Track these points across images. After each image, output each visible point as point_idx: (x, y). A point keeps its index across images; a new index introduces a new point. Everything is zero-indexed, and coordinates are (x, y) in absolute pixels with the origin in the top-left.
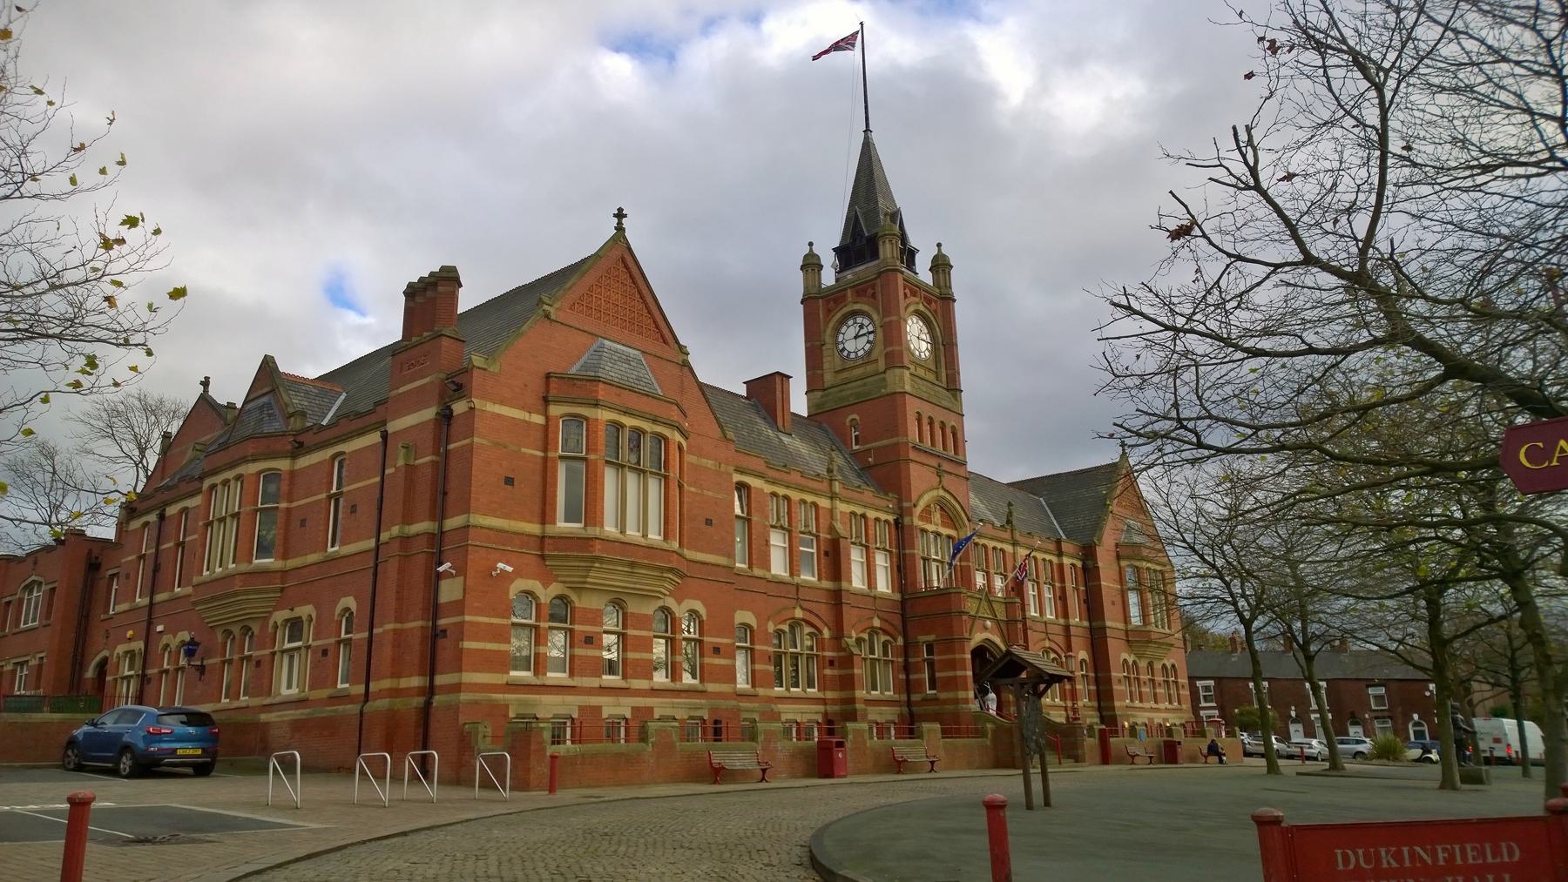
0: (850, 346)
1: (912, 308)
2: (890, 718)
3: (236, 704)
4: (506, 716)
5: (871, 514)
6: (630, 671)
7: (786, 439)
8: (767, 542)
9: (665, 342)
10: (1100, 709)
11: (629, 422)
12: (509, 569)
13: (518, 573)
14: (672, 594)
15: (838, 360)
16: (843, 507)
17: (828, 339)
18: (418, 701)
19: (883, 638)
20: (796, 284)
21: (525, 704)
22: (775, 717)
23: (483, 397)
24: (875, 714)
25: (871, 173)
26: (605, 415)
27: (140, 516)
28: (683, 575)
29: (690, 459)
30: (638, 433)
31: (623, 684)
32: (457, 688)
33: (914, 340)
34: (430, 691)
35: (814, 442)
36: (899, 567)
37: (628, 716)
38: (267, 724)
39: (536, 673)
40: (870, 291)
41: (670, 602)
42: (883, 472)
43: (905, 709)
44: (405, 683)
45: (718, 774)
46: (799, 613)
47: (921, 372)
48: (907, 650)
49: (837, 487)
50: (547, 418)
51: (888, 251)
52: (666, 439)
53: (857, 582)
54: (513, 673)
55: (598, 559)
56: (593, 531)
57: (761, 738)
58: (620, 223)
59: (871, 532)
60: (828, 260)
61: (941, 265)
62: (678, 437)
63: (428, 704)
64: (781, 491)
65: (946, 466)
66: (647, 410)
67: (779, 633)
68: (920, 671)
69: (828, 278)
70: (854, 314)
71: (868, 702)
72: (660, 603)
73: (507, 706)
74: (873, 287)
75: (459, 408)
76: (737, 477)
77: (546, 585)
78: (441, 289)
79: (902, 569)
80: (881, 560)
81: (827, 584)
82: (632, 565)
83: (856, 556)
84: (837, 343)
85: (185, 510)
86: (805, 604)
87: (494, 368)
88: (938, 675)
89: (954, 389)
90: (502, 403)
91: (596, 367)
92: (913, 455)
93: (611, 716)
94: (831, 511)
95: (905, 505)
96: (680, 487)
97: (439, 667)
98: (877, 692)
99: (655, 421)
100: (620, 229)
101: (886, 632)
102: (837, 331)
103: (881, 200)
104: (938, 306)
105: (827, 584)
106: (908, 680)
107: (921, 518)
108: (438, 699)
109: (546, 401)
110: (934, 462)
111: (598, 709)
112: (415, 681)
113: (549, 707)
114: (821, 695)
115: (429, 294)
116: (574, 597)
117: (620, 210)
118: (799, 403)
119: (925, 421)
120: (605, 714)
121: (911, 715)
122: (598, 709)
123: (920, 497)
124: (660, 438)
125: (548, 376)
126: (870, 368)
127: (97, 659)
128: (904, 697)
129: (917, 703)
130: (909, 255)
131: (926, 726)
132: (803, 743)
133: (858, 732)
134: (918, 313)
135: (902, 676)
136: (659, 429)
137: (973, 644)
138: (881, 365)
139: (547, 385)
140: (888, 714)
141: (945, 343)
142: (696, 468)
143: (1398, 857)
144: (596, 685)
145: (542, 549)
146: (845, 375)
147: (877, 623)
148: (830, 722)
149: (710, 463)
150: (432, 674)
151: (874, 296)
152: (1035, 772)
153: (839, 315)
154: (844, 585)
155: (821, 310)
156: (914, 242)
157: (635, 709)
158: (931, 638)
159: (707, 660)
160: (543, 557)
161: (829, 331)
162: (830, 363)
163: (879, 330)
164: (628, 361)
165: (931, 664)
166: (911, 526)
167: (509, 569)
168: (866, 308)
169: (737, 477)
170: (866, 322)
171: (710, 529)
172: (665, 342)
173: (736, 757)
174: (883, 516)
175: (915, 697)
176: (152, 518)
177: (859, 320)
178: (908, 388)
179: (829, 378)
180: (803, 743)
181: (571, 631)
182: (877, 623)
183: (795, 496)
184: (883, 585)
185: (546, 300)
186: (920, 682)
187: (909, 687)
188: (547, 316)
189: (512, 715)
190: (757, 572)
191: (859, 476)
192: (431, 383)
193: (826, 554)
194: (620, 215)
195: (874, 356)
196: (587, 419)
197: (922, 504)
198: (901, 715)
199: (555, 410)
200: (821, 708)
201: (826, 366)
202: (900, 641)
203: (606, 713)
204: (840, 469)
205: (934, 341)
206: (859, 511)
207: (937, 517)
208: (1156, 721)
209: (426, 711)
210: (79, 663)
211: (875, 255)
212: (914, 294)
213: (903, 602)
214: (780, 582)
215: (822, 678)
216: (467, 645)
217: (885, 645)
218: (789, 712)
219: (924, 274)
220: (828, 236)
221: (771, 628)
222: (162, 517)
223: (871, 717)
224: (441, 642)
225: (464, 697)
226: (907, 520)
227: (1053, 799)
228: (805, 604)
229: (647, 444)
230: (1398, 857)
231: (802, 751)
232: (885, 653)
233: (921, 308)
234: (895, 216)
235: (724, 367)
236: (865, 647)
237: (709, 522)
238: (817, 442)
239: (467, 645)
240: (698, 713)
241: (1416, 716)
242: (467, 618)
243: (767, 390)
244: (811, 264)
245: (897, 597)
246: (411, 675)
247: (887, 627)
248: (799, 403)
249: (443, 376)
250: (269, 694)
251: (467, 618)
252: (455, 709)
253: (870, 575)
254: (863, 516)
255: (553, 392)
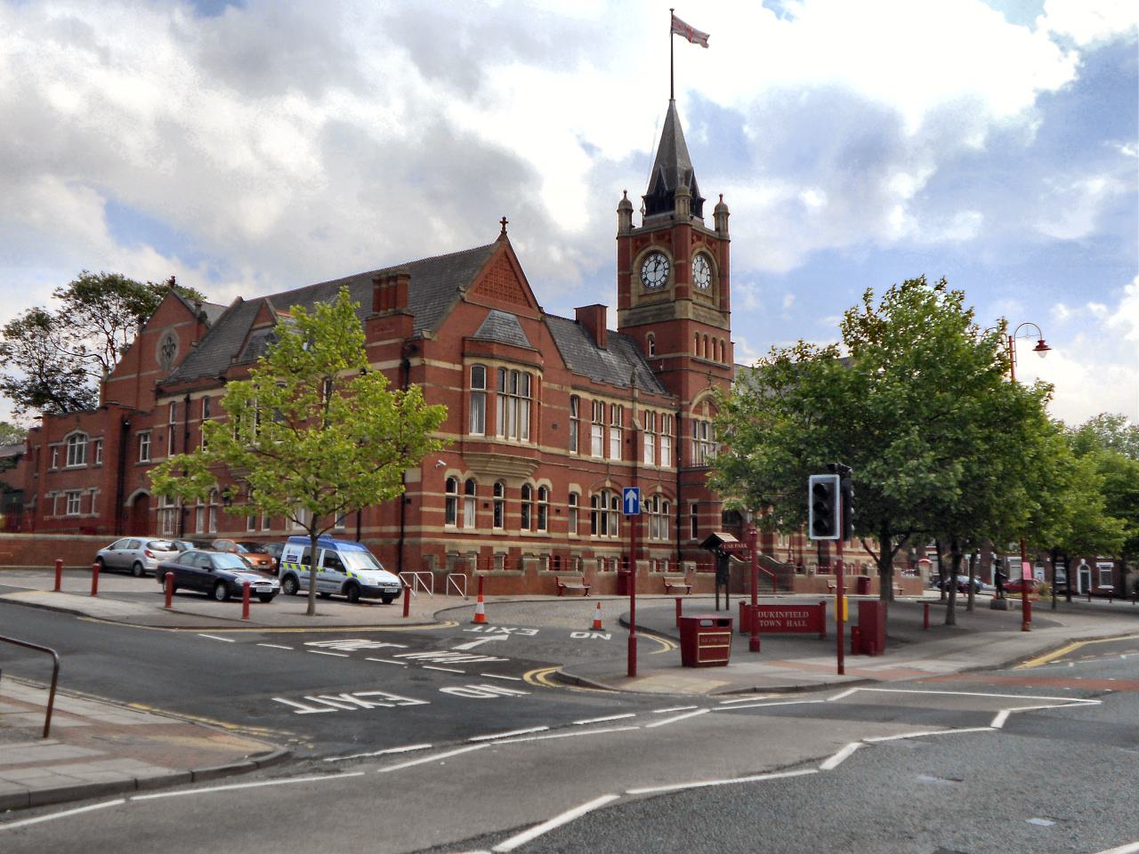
0: (651, 277)
1: (697, 251)
2: (665, 556)
3: (259, 534)
4: (443, 551)
5: (660, 411)
6: (508, 525)
7: (602, 354)
8: (590, 435)
9: (530, 306)
10: (819, 553)
11: (511, 367)
12: (444, 464)
13: (450, 465)
14: (532, 475)
15: (641, 287)
16: (640, 407)
17: (635, 270)
18: (395, 541)
19: (664, 500)
20: (613, 224)
21: (453, 544)
22: (590, 555)
23: (430, 358)
24: (655, 553)
25: (673, 118)
26: (497, 364)
27: (169, 395)
28: (538, 467)
29: (544, 384)
30: (515, 373)
31: (503, 533)
32: (419, 534)
33: (697, 274)
34: (402, 535)
35: (621, 353)
36: (677, 448)
37: (507, 553)
38: (849, 617)
39: (458, 526)
40: (667, 237)
41: (531, 481)
42: (669, 378)
43: (676, 551)
44: (385, 529)
45: (561, 591)
46: (608, 484)
47: (701, 300)
48: (680, 508)
49: (637, 393)
50: (464, 366)
51: (682, 208)
52: (531, 375)
53: (648, 461)
54: (446, 525)
55: (493, 456)
56: (490, 439)
57: (585, 569)
58: (504, 228)
59: (659, 424)
60: (638, 205)
61: (721, 213)
62: (538, 373)
63: (401, 543)
64: (600, 399)
65: (715, 372)
66: (521, 358)
67: (594, 499)
68: (688, 524)
69: (637, 220)
70: (655, 253)
71: (651, 545)
72: (525, 481)
73: (444, 546)
74: (670, 234)
75: (415, 362)
76: (573, 392)
77: (463, 472)
78: (399, 282)
79: (679, 450)
80: (665, 443)
81: (628, 463)
82: (512, 459)
83: (648, 441)
84: (641, 274)
85: (207, 399)
86: (613, 478)
87: (435, 339)
88: (699, 527)
89: (724, 311)
90: (439, 359)
91: (491, 331)
92: (691, 366)
93: (498, 553)
94: (632, 411)
95: (684, 403)
96: (539, 404)
97: (407, 521)
98: (659, 532)
99: (526, 365)
100: (504, 232)
101: (665, 496)
102: (642, 264)
103: (679, 160)
104: (718, 244)
105: (628, 463)
106: (679, 530)
107: (695, 411)
108: (406, 540)
109: (463, 355)
110: (706, 370)
111: (490, 548)
112: (393, 529)
113: (465, 545)
114: (620, 540)
115: (391, 283)
116: (478, 479)
117: (504, 219)
118: (612, 322)
119: (702, 338)
120: (494, 552)
121: (680, 554)
122: (490, 548)
123: (694, 397)
124: (527, 375)
125: (464, 339)
126: (664, 296)
127: (136, 493)
128: (675, 542)
129: (684, 547)
130: (697, 204)
131: (686, 563)
132: (610, 573)
133: (644, 568)
134: (702, 254)
135: (675, 527)
136: (528, 370)
137: (724, 507)
138: (672, 296)
139: (463, 345)
140: (666, 553)
141: (720, 277)
142: (548, 391)
143: (775, 614)
144: (490, 533)
145: (461, 450)
146: (646, 299)
147: (659, 489)
148: (625, 559)
149: (555, 386)
150: (403, 524)
151: (670, 241)
152: (722, 596)
153: (643, 253)
154: (639, 464)
155: (632, 245)
156: (703, 192)
157: (511, 549)
158: (696, 501)
159: (552, 518)
160: (462, 455)
161: (636, 264)
162: (635, 289)
163: (672, 269)
164: (508, 324)
165: (695, 520)
166: (687, 419)
167: (444, 464)
168: (663, 250)
169: (573, 392)
170: (663, 260)
171: (556, 432)
172: (530, 306)
173: (572, 580)
174: (668, 412)
175: (683, 542)
176: (180, 399)
177: (652, 258)
178: (690, 316)
179: (634, 301)
180: (610, 573)
181: (476, 500)
182: (659, 489)
183: (609, 401)
184: (666, 463)
185: (462, 289)
186: (687, 532)
187: (679, 535)
188: (463, 300)
189: (446, 551)
190: (584, 457)
191: (653, 379)
192: (396, 344)
193: (628, 441)
194: (504, 222)
195: (667, 287)
196: (487, 367)
197: (696, 402)
198: (673, 555)
199: (469, 362)
200: (620, 549)
201: (633, 291)
202: (675, 502)
203: (495, 551)
204: (640, 376)
205: (712, 274)
206: (651, 409)
207: (706, 410)
208: (862, 562)
209: (400, 546)
210: (121, 496)
211: (672, 207)
212: (699, 239)
213: (679, 474)
214: (596, 464)
215: (622, 528)
216: (425, 509)
217: (664, 505)
218: (600, 551)
219: (709, 222)
220: (638, 190)
221: (590, 494)
222: (188, 400)
223: (652, 556)
224: (408, 506)
225: (423, 540)
226: (684, 414)
227: (730, 608)
228: (613, 478)
229: (520, 380)
230: (775, 614)
231: (608, 578)
232: (665, 511)
233: (704, 249)
234: (689, 177)
235: (559, 302)
236: (651, 506)
237: (554, 426)
238: (623, 353)
239: (425, 509)
240: (546, 552)
241: (1083, 561)
242: (424, 493)
243: (590, 318)
244: (625, 209)
245: (675, 470)
246: (389, 525)
247: (666, 492)
248: (612, 322)
249: (403, 340)
250: (284, 529)
251: (424, 493)
252: (419, 547)
253: (657, 455)
254: (654, 412)
255: (467, 350)
